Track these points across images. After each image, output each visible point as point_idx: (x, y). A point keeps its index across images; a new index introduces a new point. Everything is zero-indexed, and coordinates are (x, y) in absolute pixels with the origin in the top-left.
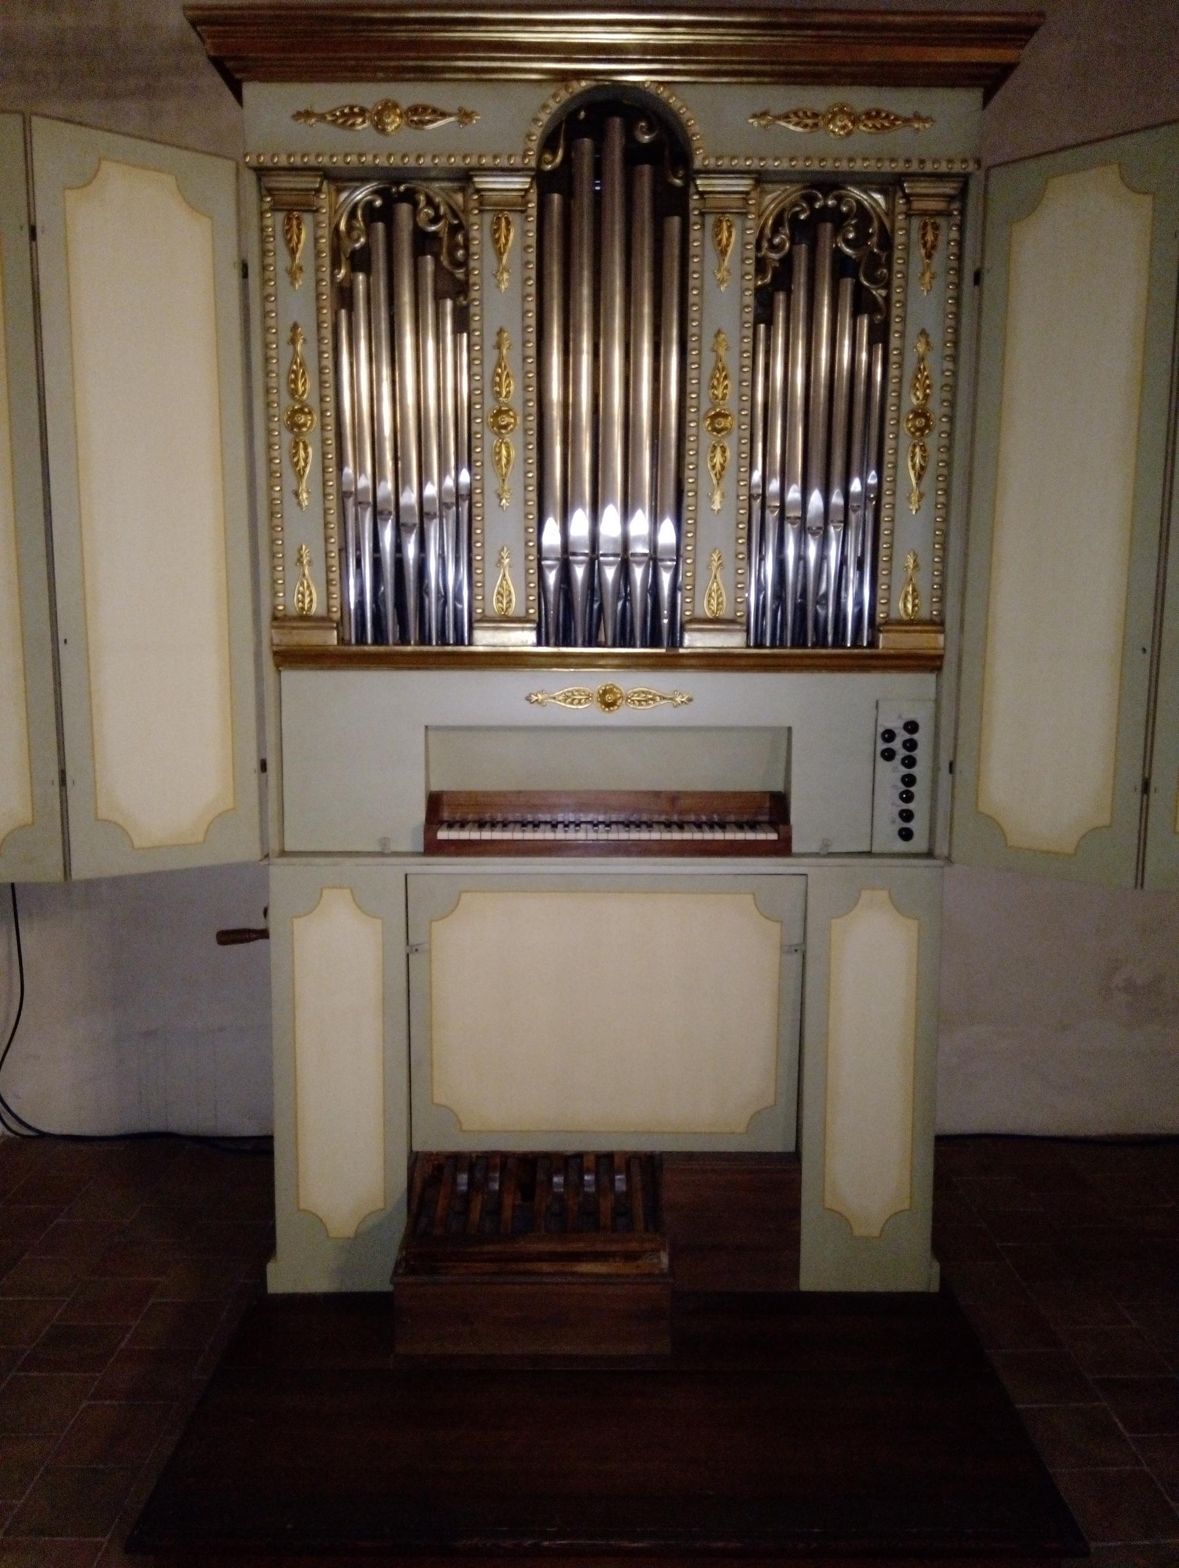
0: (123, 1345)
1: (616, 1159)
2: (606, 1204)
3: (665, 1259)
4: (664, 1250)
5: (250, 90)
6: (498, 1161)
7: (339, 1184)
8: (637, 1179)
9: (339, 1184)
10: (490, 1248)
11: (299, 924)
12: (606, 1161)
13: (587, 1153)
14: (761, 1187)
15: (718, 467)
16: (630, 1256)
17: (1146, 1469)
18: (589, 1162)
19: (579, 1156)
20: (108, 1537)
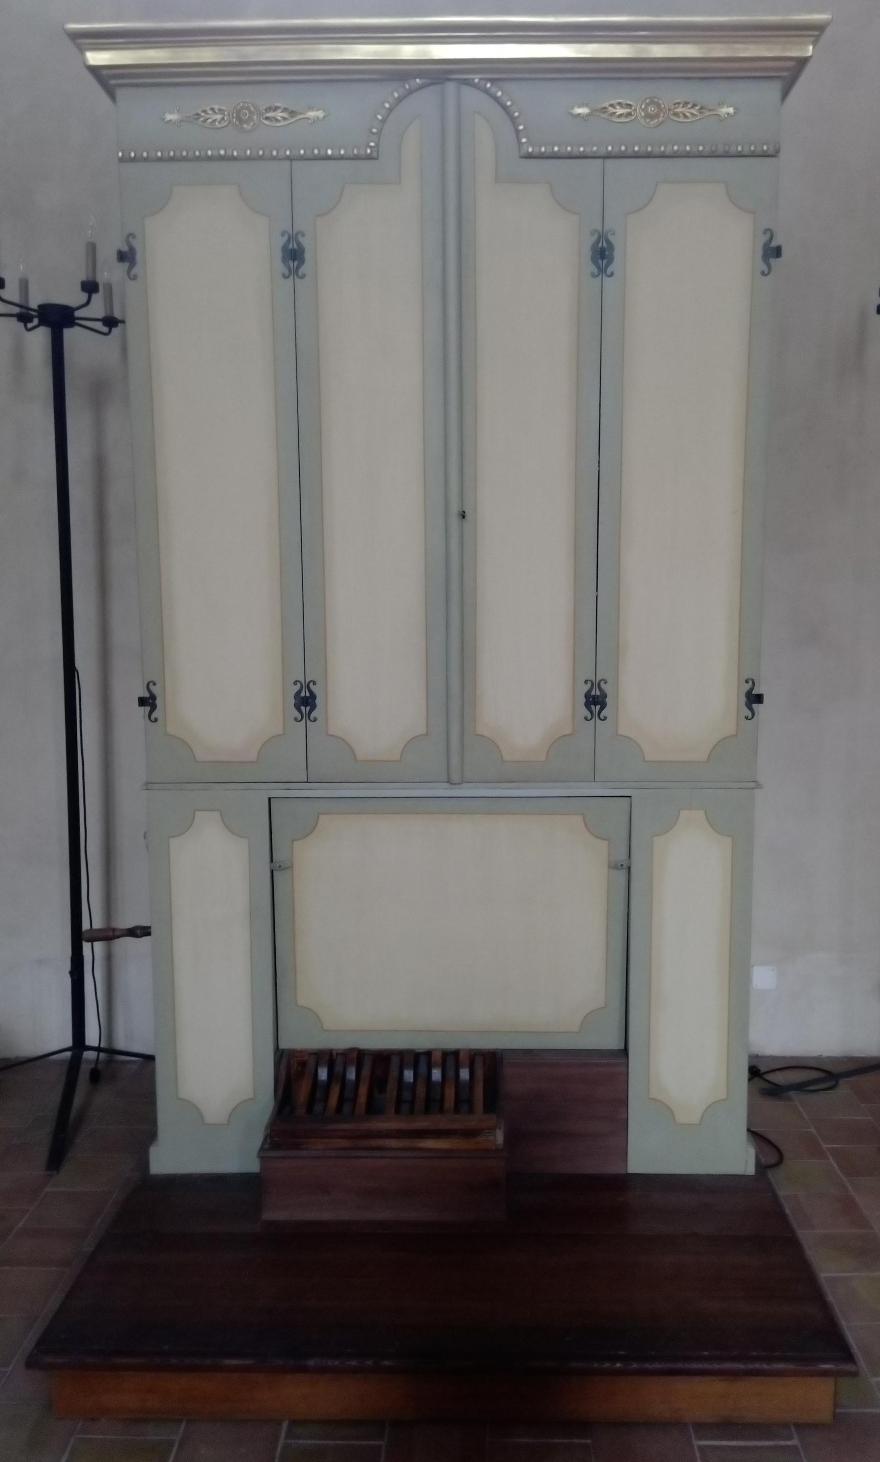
0: (20, 1225)
1: (462, 1055)
2: (450, 1093)
3: (499, 1137)
4: (500, 1129)
5: (120, 93)
6: (355, 1055)
7: (213, 1093)
8: (480, 1072)
9: (213, 1093)
10: (346, 1126)
11: (174, 843)
12: (451, 1058)
13: (436, 1050)
14: (590, 1083)
15: (285, 115)
16: (470, 1134)
17: (813, 1130)
18: (437, 1057)
19: (428, 1054)
20: (10, 1368)
